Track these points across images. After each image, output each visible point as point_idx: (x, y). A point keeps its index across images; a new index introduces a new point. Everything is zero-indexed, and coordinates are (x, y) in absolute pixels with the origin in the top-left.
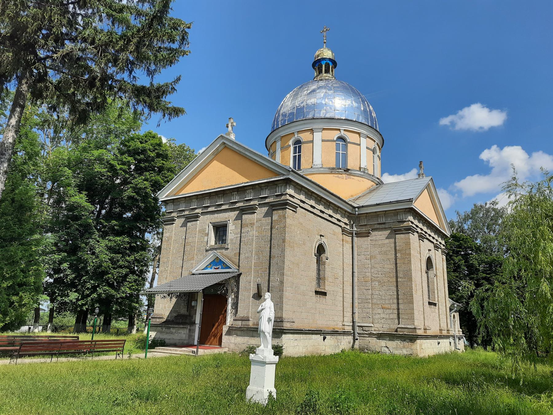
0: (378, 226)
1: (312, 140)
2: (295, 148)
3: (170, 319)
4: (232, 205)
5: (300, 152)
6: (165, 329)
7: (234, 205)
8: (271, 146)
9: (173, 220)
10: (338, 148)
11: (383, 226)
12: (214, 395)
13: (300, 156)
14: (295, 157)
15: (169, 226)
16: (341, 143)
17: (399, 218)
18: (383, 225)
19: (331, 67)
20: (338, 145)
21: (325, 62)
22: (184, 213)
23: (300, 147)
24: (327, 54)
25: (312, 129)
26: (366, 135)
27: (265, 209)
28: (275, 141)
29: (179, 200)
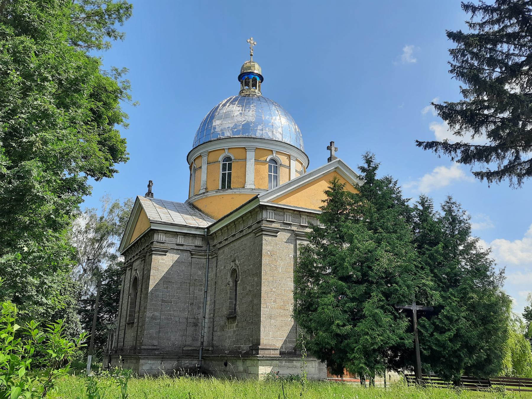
0: (176, 247)
1: (244, 158)
2: (224, 165)
3: (284, 350)
4: (301, 228)
5: (230, 169)
6: (285, 362)
7: (304, 228)
8: (194, 160)
9: (276, 232)
10: (270, 171)
11: (181, 248)
12: (128, 362)
13: (230, 175)
14: (224, 175)
15: (270, 238)
16: (273, 165)
17: (178, 242)
18: (162, 245)
19: (258, 82)
20: (270, 167)
21: (253, 76)
22: (290, 227)
23: (230, 165)
24: (257, 70)
25: (245, 148)
26: (295, 158)
27: (287, 235)
28: (200, 156)
29: (285, 210)
